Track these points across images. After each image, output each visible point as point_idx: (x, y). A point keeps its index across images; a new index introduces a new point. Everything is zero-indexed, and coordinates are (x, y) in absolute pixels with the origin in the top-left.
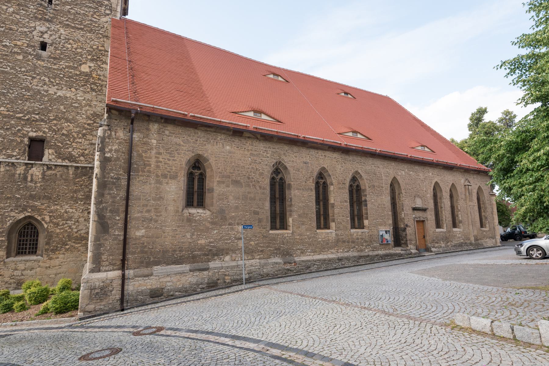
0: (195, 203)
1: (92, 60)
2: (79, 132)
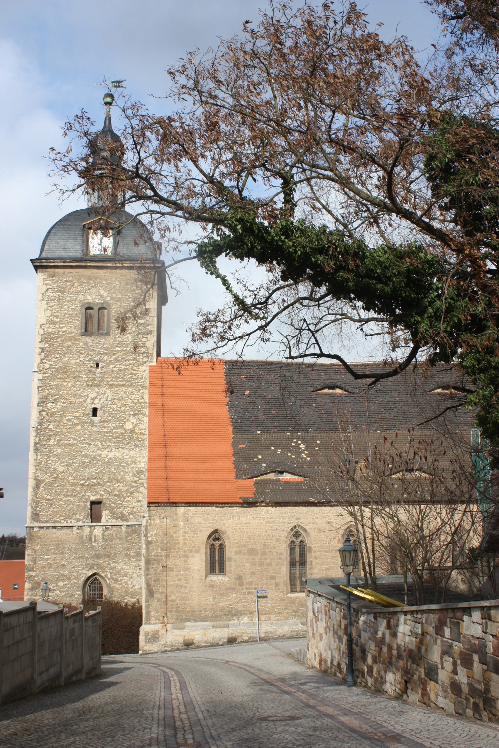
0: (217, 571)
1: (134, 415)
2: (127, 491)
